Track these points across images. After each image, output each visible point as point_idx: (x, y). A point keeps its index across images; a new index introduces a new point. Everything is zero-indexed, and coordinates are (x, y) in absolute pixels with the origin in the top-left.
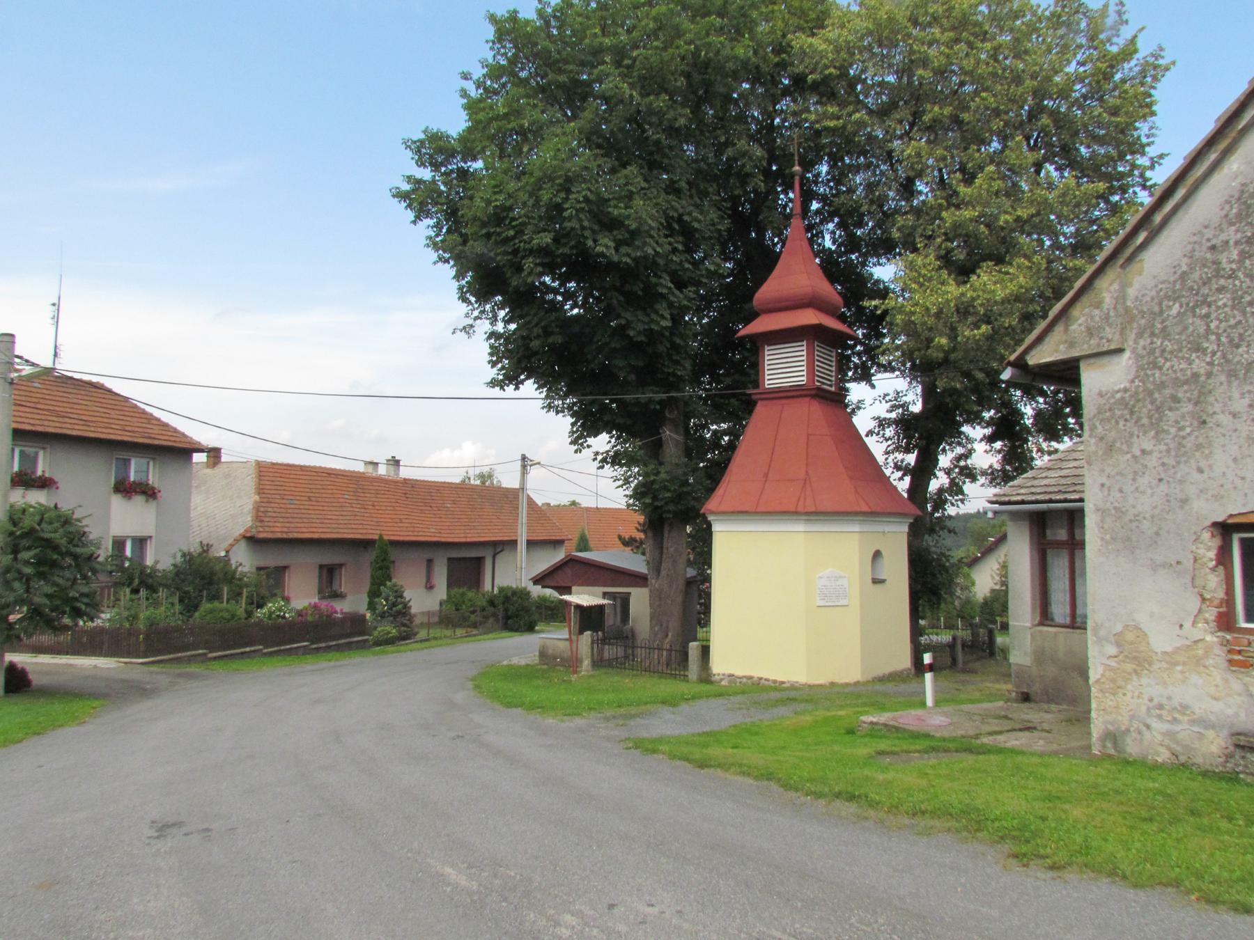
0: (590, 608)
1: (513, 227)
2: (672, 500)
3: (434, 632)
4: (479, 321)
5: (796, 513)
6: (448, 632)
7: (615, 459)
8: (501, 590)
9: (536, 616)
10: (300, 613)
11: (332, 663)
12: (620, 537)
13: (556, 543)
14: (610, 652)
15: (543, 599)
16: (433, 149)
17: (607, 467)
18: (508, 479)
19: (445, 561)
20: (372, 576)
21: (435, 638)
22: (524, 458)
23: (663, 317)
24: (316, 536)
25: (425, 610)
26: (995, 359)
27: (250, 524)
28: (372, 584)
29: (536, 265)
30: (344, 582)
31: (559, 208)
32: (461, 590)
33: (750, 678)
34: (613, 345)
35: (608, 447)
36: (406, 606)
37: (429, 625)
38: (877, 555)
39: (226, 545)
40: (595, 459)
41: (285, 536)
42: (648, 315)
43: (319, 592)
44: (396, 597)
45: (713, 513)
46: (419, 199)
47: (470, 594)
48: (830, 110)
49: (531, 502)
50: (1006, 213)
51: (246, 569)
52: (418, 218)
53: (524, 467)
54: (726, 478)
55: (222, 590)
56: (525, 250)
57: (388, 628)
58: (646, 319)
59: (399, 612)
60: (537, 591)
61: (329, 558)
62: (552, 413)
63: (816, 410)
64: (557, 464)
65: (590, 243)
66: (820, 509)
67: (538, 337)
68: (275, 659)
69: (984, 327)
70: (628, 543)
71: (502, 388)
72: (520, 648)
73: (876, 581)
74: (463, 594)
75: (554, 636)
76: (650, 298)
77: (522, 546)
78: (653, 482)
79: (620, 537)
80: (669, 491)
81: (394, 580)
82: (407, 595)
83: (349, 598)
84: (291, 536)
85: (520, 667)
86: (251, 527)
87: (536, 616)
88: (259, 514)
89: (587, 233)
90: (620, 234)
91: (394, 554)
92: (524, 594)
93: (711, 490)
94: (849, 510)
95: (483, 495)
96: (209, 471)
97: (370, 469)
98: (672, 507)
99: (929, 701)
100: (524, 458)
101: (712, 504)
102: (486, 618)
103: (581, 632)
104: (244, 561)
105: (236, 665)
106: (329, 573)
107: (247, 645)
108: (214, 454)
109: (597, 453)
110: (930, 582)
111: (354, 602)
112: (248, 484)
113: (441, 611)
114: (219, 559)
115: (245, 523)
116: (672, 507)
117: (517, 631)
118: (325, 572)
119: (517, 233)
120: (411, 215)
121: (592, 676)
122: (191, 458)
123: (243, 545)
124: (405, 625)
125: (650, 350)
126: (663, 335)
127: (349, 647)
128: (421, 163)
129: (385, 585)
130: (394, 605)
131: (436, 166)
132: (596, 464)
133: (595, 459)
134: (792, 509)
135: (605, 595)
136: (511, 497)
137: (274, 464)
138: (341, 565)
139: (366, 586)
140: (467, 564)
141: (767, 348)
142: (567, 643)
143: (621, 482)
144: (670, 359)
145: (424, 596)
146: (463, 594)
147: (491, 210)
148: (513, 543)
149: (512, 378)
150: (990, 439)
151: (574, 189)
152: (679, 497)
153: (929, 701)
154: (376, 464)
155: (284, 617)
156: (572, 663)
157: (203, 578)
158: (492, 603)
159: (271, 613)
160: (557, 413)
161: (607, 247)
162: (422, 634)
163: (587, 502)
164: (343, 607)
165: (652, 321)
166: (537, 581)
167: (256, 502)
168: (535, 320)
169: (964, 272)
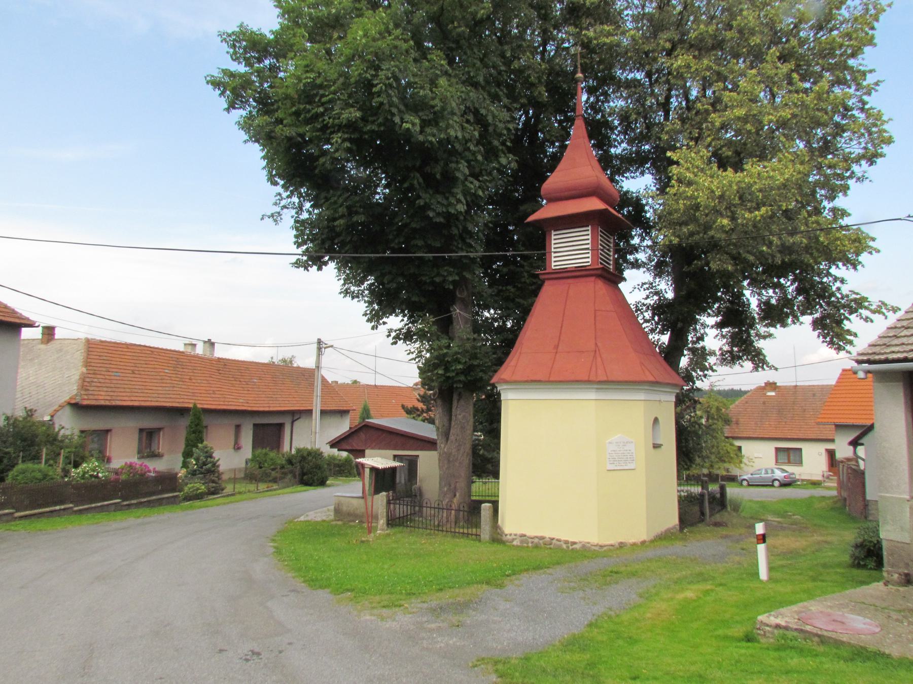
0: (384, 470)
1: (323, 104)
2: (464, 372)
3: (240, 487)
4: (285, 210)
5: (589, 382)
6: (252, 487)
7: (408, 336)
8: (299, 450)
9: (328, 473)
10: (117, 472)
11: (140, 521)
12: (403, 407)
13: (343, 413)
14: (400, 510)
15: (332, 458)
16: (250, 45)
17: (400, 342)
18: (306, 360)
19: (251, 426)
20: (187, 440)
21: (240, 493)
22: (319, 342)
23: (459, 201)
24: (136, 404)
25: (233, 467)
26: (764, 244)
27: (75, 392)
28: (187, 445)
29: (344, 140)
30: (162, 444)
31: (369, 85)
32: (264, 451)
33: (542, 538)
34: (414, 225)
35: (400, 325)
36: (214, 464)
37: (234, 480)
38: (656, 420)
39: (51, 410)
40: (389, 336)
41: (107, 403)
42: (447, 199)
43: (139, 453)
44: (207, 457)
45: (506, 382)
46: (234, 90)
47: (272, 454)
48: (606, 27)
49: (324, 380)
50: (769, 114)
51: (68, 433)
52: (232, 106)
53: (319, 349)
54: (513, 351)
55: (41, 450)
56: (333, 126)
57: (197, 485)
58: (445, 202)
59: (208, 471)
60: (329, 452)
61: (149, 423)
62: (348, 298)
63: (600, 286)
64: (353, 343)
65: (397, 120)
66: (610, 379)
67: (342, 217)
68: (84, 517)
69: (763, 210)
70: (411, 412)
71: (306, 268)
72: (316, 503)
73: (656, 446)
74: (266, 454)
75: (348, 491)
76: (448, 182)
77: (316, 414)
78: (445, 355)
79: (403, 407)
80: (459, 363)
81: (205, 443)
82: (216, 455)
83: (165, 458)
84: (114, 403)
85: (317, 522)
86: (76, 395)
87: (328, 473)
88: (84, 383)
89: (394, 110)
90: (426, 115)
91: (206, 420)
92: (317, 454)
93: (500, 362)
94: (637, 379)
95: (283, 373)
96: (43, 346)
97: (189, 349)
98: (462, 378)
99: (763, 574)
100: (319, 342)
101: (505, 372)
102: (285, 474)
103: (377, 491)
104: (68, 426)
105: (40, 524)
106: (148, 436)
107: (56, 504)
108: (49, 332)
109: (390, 331)
110: (691, 445)
111: (169, 461)
112: (78, 357)
113: (246, 468)
114: (43, 423)
115: (70, 390)
116: (462, 378)
117: (311, 485)
118: (144, 434)
119: (326, 110)
120: (223, 103)
121: (388, 535)
122: (20, 332)
123: (68, 410)
124: (213, 482)
125: (445, 232)
126: (457, 219)
127: (160, 503)
128: (235, 58)
129: (197, 447)
130: (205, 464)
131: (249, 64)
132: (390, 340)
133: (389, 336)
134: (586, 379)
135: (395, 457)
136: (308, 376)
137: (102, 341)
138: (160, 429)
139: (182, 446)
140: (269, 430)
141: (553, 233)
142: (362, 501)
143: (414, 356)
144: (463, 240)
145: (231, 455)
146: (266, 454)
147: (301, 86)
148: (309, 412)
149: (315, 260)
150: (720, 325)
151: (383, 67)
152: (469, 369)
153: (763, 574)
154: (195, 345)
155: (97, 477)
156: (367, 519)
157: (24, 440)
158: (290, 462)
159: (85, 473)
160: (353, 298)
161: (413, 124)
162: (229, 488)
163: (367, 379)
164: (156, 466)
165: (450, 204)
166: (334, 444)
167: (83, 373)
168: (341, 200)
169: (738, 167)
